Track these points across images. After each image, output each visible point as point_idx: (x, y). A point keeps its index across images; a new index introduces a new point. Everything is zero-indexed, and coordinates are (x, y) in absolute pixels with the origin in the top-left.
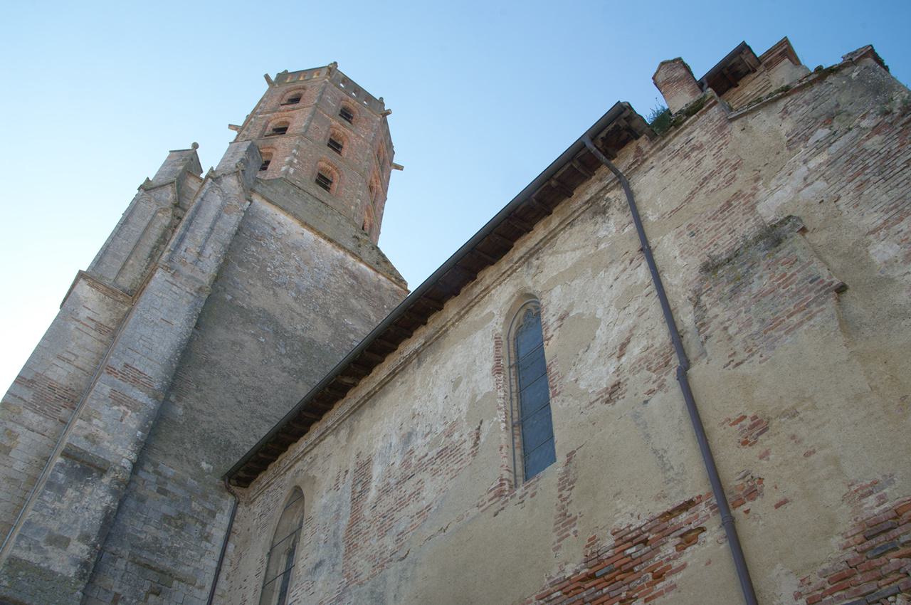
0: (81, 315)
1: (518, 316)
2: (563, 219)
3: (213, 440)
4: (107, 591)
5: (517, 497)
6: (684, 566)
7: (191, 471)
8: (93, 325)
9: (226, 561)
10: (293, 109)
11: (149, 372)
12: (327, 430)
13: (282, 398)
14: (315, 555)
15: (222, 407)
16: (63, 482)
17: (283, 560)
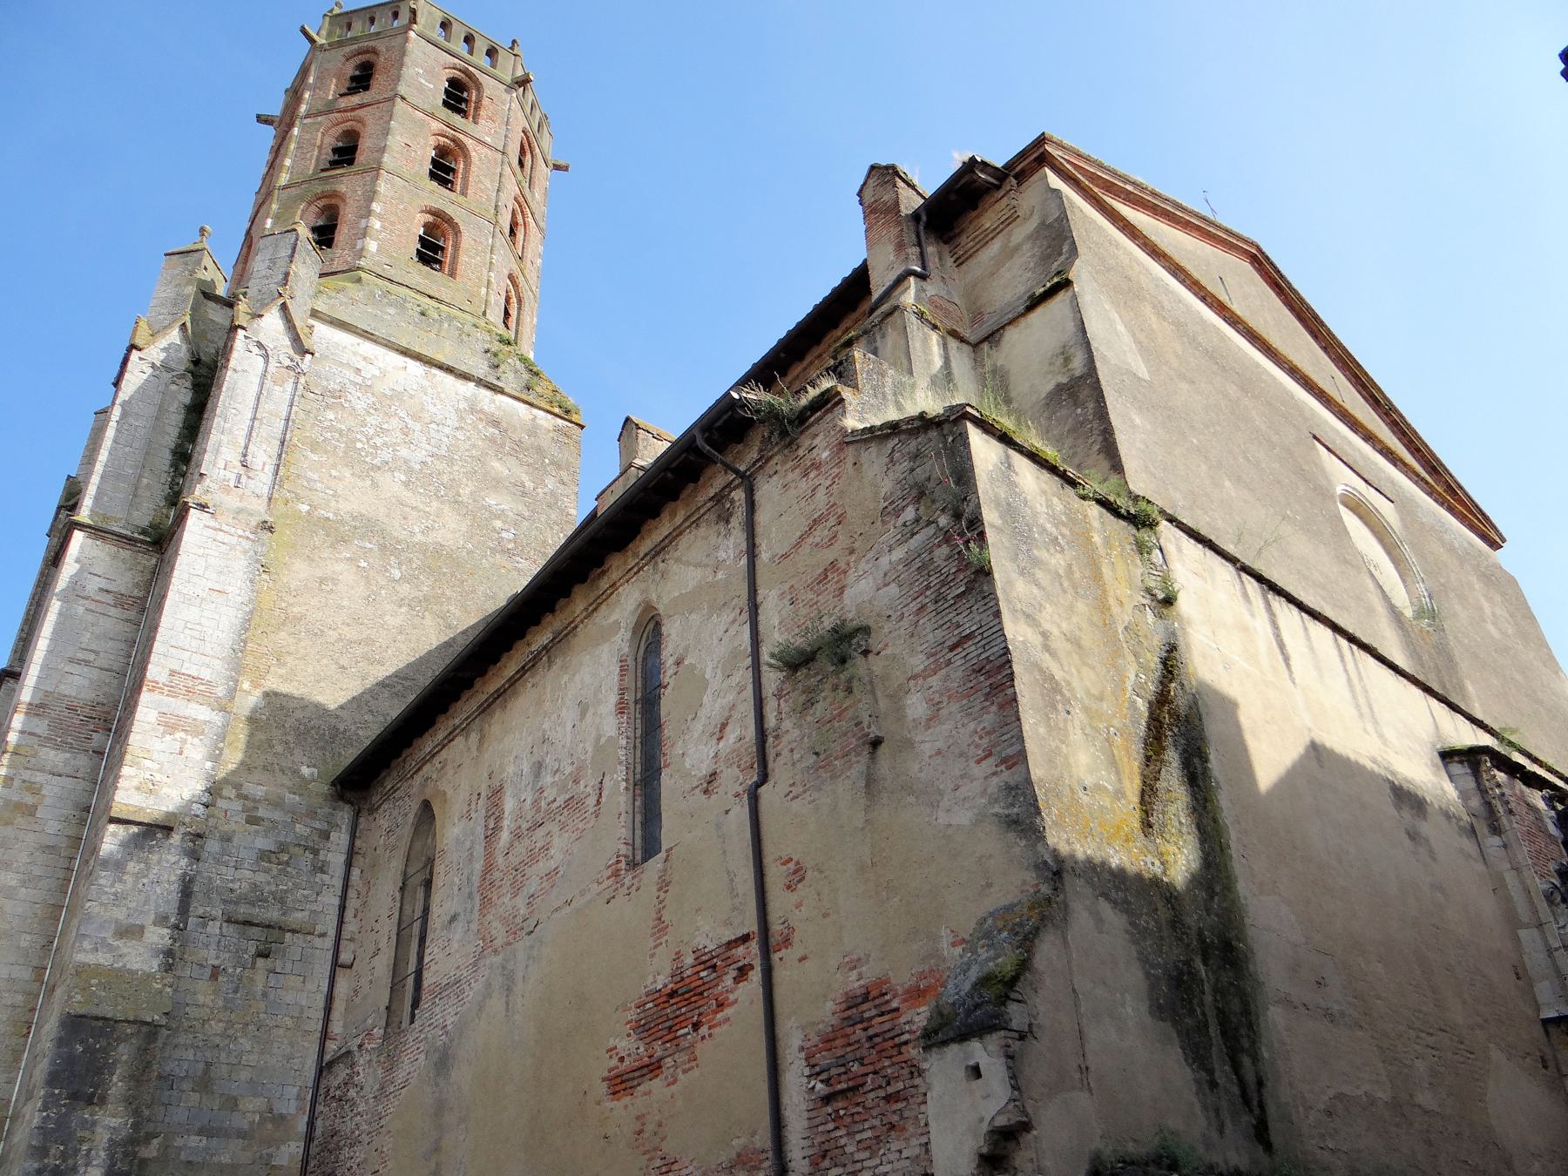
0: (88, 588)
1: (648, 628)
2: (688, 513)
3: (313, 732)
4: (201, 966)
5: (626, 887)
6: (736, 1001)
7: (289, 783)
8: (109, 599)
9: (352, 894)
10: (362, 106)
11: (206, 674)
12: (455, 729)
13: (403, 647)
14: (449, 903)
15: (318, 682)
16: (119, 856)
17: (420, 894)
